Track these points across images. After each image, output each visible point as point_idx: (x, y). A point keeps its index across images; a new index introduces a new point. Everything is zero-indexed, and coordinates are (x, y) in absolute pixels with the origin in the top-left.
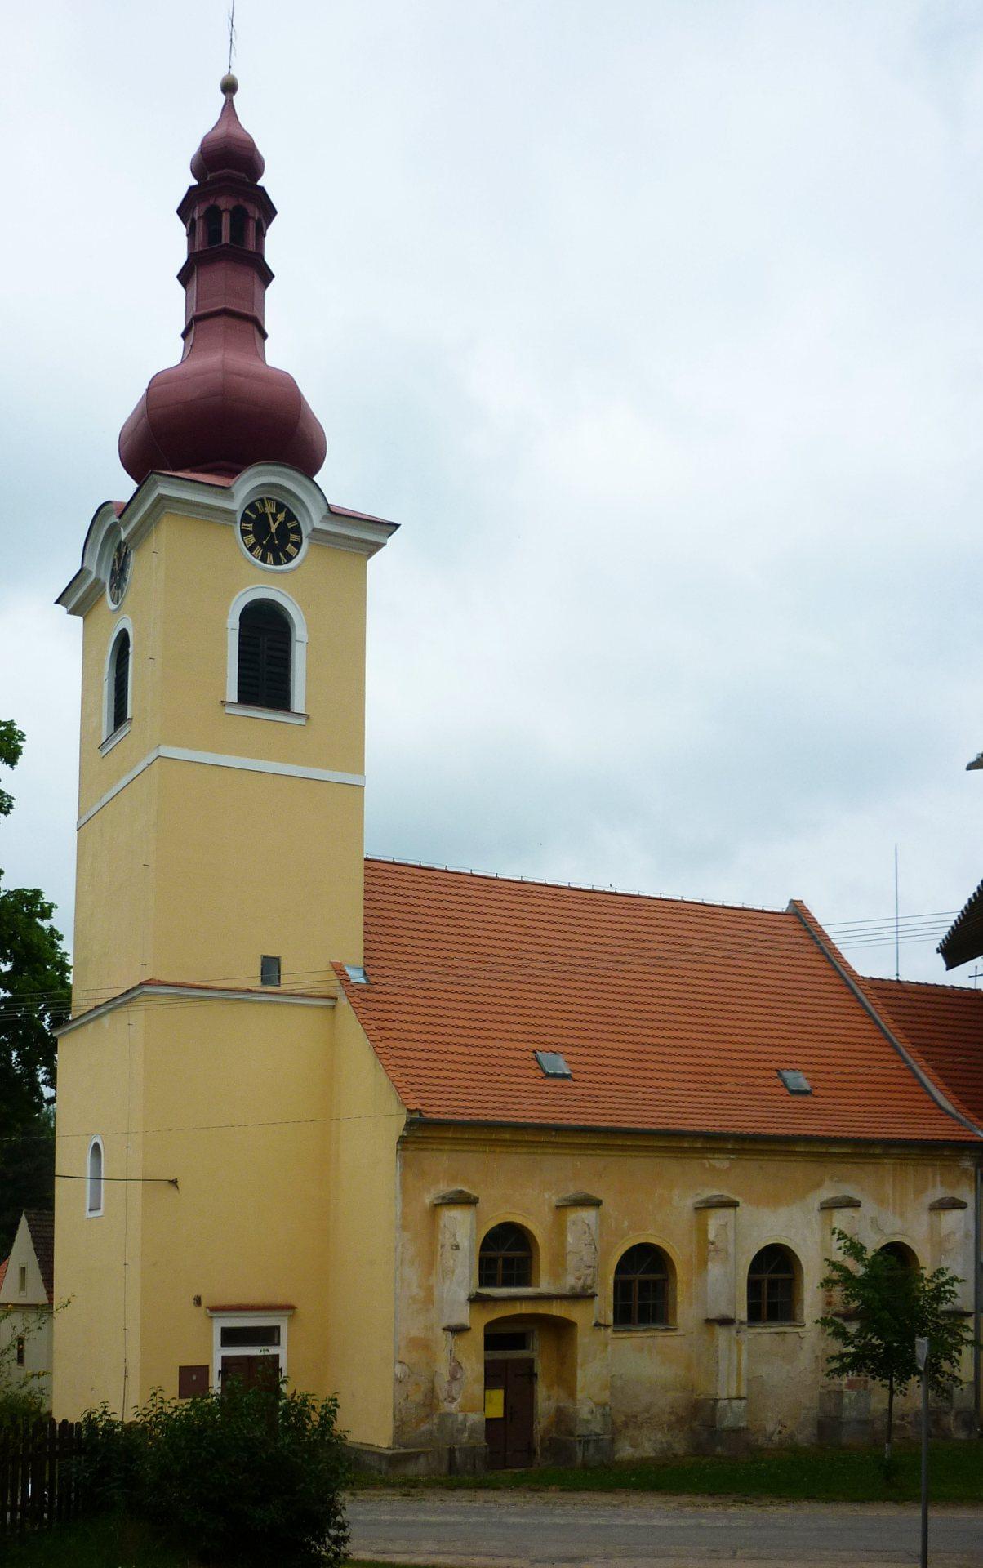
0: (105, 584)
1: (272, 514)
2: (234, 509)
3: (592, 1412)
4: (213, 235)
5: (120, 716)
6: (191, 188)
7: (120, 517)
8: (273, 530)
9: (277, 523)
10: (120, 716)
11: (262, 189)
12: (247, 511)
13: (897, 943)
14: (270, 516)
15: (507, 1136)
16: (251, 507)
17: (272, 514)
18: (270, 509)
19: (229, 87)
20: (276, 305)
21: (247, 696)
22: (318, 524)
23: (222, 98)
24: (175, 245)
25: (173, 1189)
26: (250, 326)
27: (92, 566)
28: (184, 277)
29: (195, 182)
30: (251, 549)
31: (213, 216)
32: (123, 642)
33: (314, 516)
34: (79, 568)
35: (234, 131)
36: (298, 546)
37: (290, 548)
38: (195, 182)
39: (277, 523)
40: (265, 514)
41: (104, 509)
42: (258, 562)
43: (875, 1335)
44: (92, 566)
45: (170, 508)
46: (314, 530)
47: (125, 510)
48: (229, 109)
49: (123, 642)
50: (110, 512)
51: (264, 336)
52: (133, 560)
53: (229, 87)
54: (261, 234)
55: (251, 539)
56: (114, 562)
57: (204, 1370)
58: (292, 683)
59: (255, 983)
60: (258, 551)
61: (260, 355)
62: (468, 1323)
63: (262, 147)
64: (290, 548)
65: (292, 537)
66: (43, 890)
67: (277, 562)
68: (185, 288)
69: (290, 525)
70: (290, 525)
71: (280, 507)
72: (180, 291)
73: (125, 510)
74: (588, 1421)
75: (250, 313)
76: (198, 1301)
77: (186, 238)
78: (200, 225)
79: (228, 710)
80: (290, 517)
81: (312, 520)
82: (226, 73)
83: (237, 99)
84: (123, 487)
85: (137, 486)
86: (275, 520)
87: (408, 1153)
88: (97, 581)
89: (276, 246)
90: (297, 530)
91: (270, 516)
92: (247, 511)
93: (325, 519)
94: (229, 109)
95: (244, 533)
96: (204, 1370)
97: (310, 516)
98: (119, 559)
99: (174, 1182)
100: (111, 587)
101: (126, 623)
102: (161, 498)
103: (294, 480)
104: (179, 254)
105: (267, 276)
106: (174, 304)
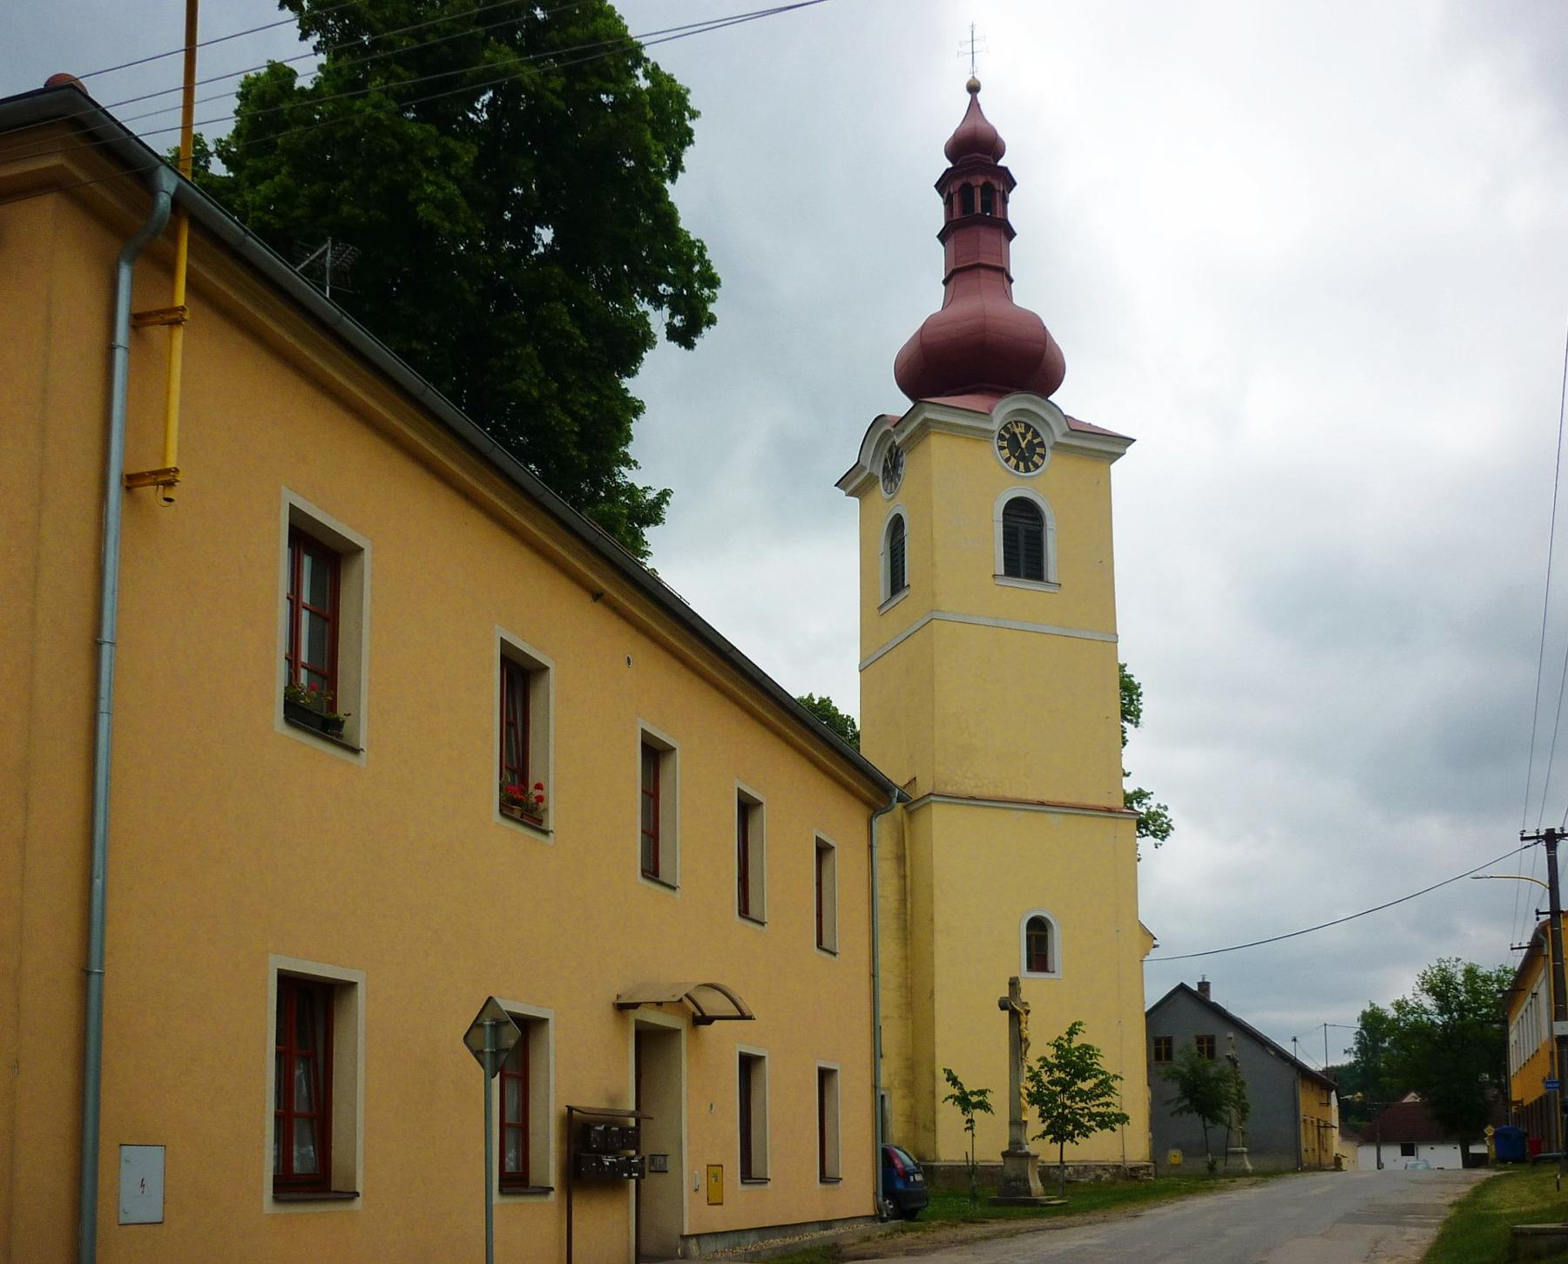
0: (878, 477)
1: (1020, 433)
2: (993, 429)
4: (967, 205)
5: (897, 583)
6: (948, 170)
7: (895, 426)
8: (1023, 445)
9: (1026, 441)
10: (897, 583)
11: (1005, 169)
12: (1003, 432)
14: (1019, 436)
16: (1005, 428)
17: (1020, 433)
18: (1019, 430)
19: (973, 89)
20: (1019, 255)
21: (1012, 569)
22: (1060, 439)
23: (968, 97)
24: (935, 212)
26: (998, 276)
27: (867, 462)
28: (943, 237)
29: (950, 165)
30: (1007, 460)
31: (966, 192)
32: (897, 524)
33: (1056, 431)
34: (856, 461)
35: (980, 124)
36: (1043, 457)
37: (1036, 458)
38: (950, 165)
39: (1026, 441)
40: (1014, 435)
41: (880, 419)
42: (1013, 470)
44: (867, 462)
45: (934, 428)
46: (1057, 444)
47: (900, 422)
48: (974, 106)
49: (897, 524)
50: (887, 422)
51: (1011, 281)
52: (905, 459)
53: (973, 89)
54: (1005, 201)
55: (1006, 453)
56: (886, 460)
58: (1045, 561)
60: (1013, 461)
61: (1008, 295)
63: (1002, 134)
64: (1036, 458)
65: (1038, 450)
66: (717, 324)
67: (1027, 470)
68: (944, 245)
69: (1035, 441)
70: (1035, 441)
71: (1028, 427)
72: (939, 248)
73: (898, 422)
75: (999, 265)
77: (943, 206)
78: (956, 199)
79: (998, 581)
80: (1036, 434)
81: (1054, 435)
82: (970, 77)
83: (980, 96)
84: (900, 404)
85: (912, 405)
86: (1024, 439)
88: (871, 474)
89: (1018, 208)
90: (1042, 445)
91: (1019, 436)
92: (1003, 432)
93: (1065, 435)
94: (974, 106)
95: (1001, 448)
97: (1052, 432)
98: (891, 459)
100: (884, 481)
101: (900, 506)
102: (926, 421)
103: (1036, 403)
104: (940, 223)
105: (1010, 234)
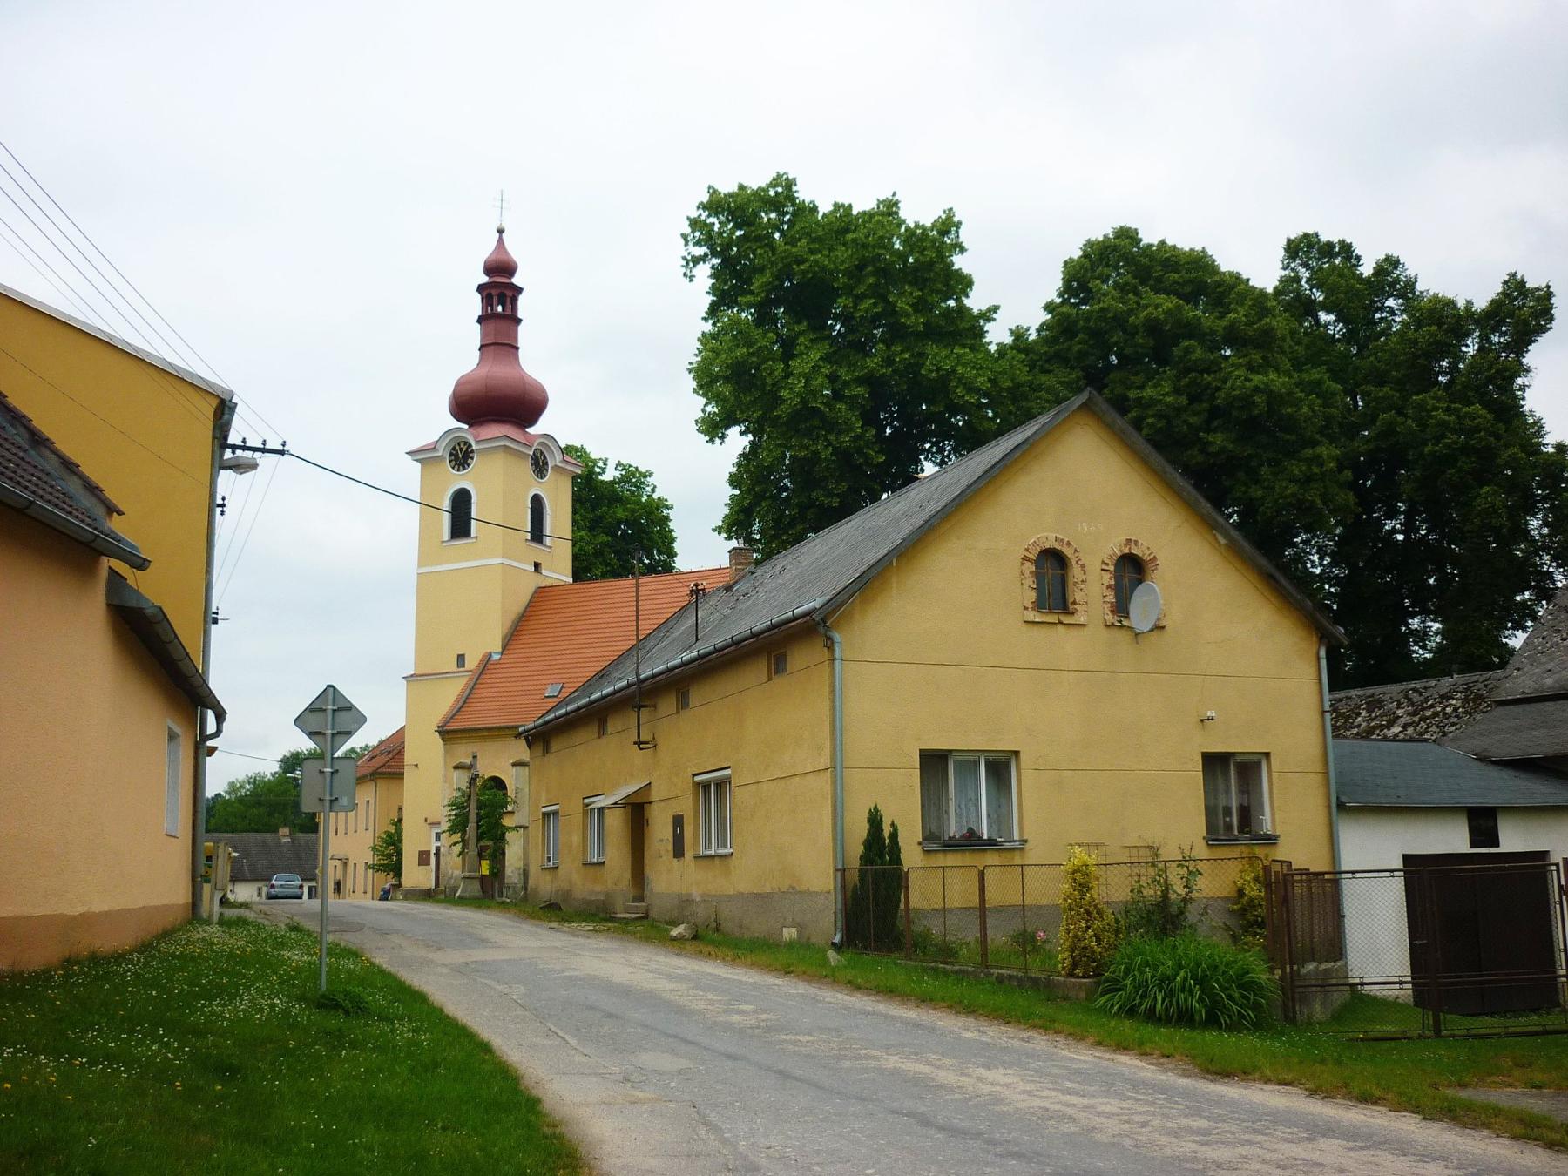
3: (512, 872)
13: (842, 660)
15: (486, 734)
19: (501, 231)
23: (498, 235)
25: (416, 769)
43: (1410, 650)
46: (556, 466)
48: (501, 241)
53: (501, 231)
57: (428, 853)
59: (455, 668)
62: (527, 825)
63: (518, 263)
74: (510, 876)
76: (426, 820)
87: (448, 746)
94: (501, 241)
95: (532, 465)
96: (428, 853)
99: (417, 765)
106: (474, 334)
